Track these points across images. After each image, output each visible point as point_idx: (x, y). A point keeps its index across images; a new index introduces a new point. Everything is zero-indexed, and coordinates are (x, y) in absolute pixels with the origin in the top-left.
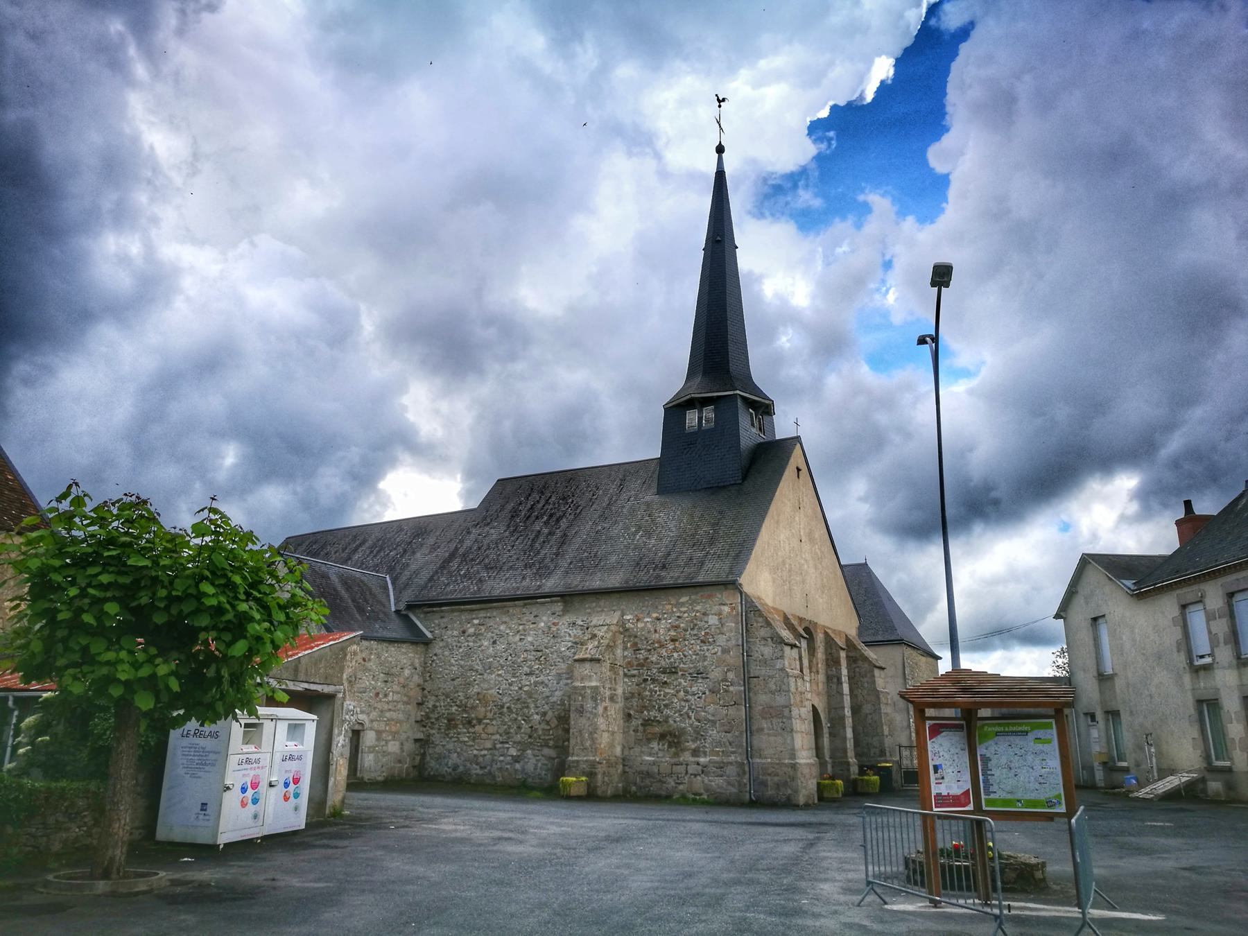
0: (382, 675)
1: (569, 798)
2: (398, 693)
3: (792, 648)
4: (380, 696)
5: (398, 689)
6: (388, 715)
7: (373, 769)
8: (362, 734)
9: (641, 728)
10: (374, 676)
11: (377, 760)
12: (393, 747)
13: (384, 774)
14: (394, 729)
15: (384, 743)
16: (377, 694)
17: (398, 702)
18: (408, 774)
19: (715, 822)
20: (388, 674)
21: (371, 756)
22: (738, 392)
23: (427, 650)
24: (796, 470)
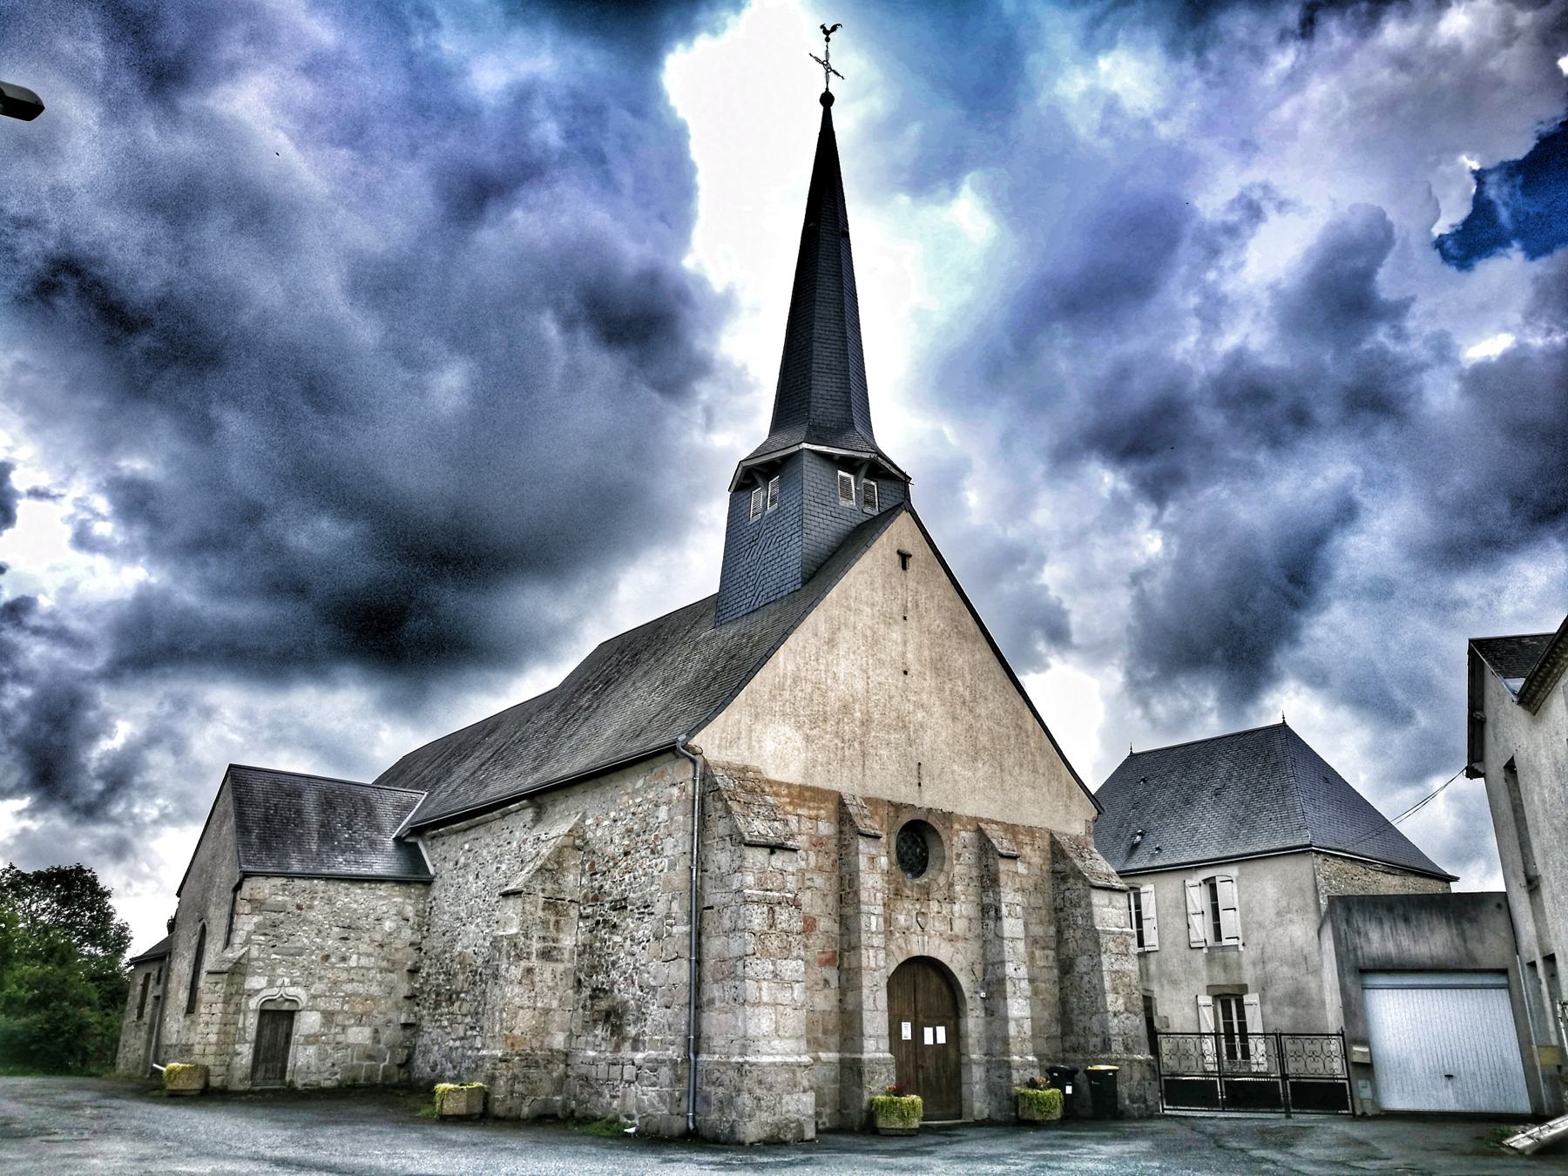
0: (337, 929)
1: (447, 1120)
2: (369, 955)
3: (772, 853)
4: (333, 960)
5: (370, 950)
6: (349, 988)
7: (313, 1069)
8: (296, 1017)
9: (589, 1003)
10: (320, 931)
11: (322, 1057)
12: (359, 1035)
13: (338, 1076)
14: (359, 1009)
15: (338, 1029)
16: (327, 958)
17: (368, 969)
18: (386, 1077)
19: (1384, 1138)
20: (349, 927)
21: (311, 1050)
22: (805, 445)
23: (427, 893)
24: (897, 558)
